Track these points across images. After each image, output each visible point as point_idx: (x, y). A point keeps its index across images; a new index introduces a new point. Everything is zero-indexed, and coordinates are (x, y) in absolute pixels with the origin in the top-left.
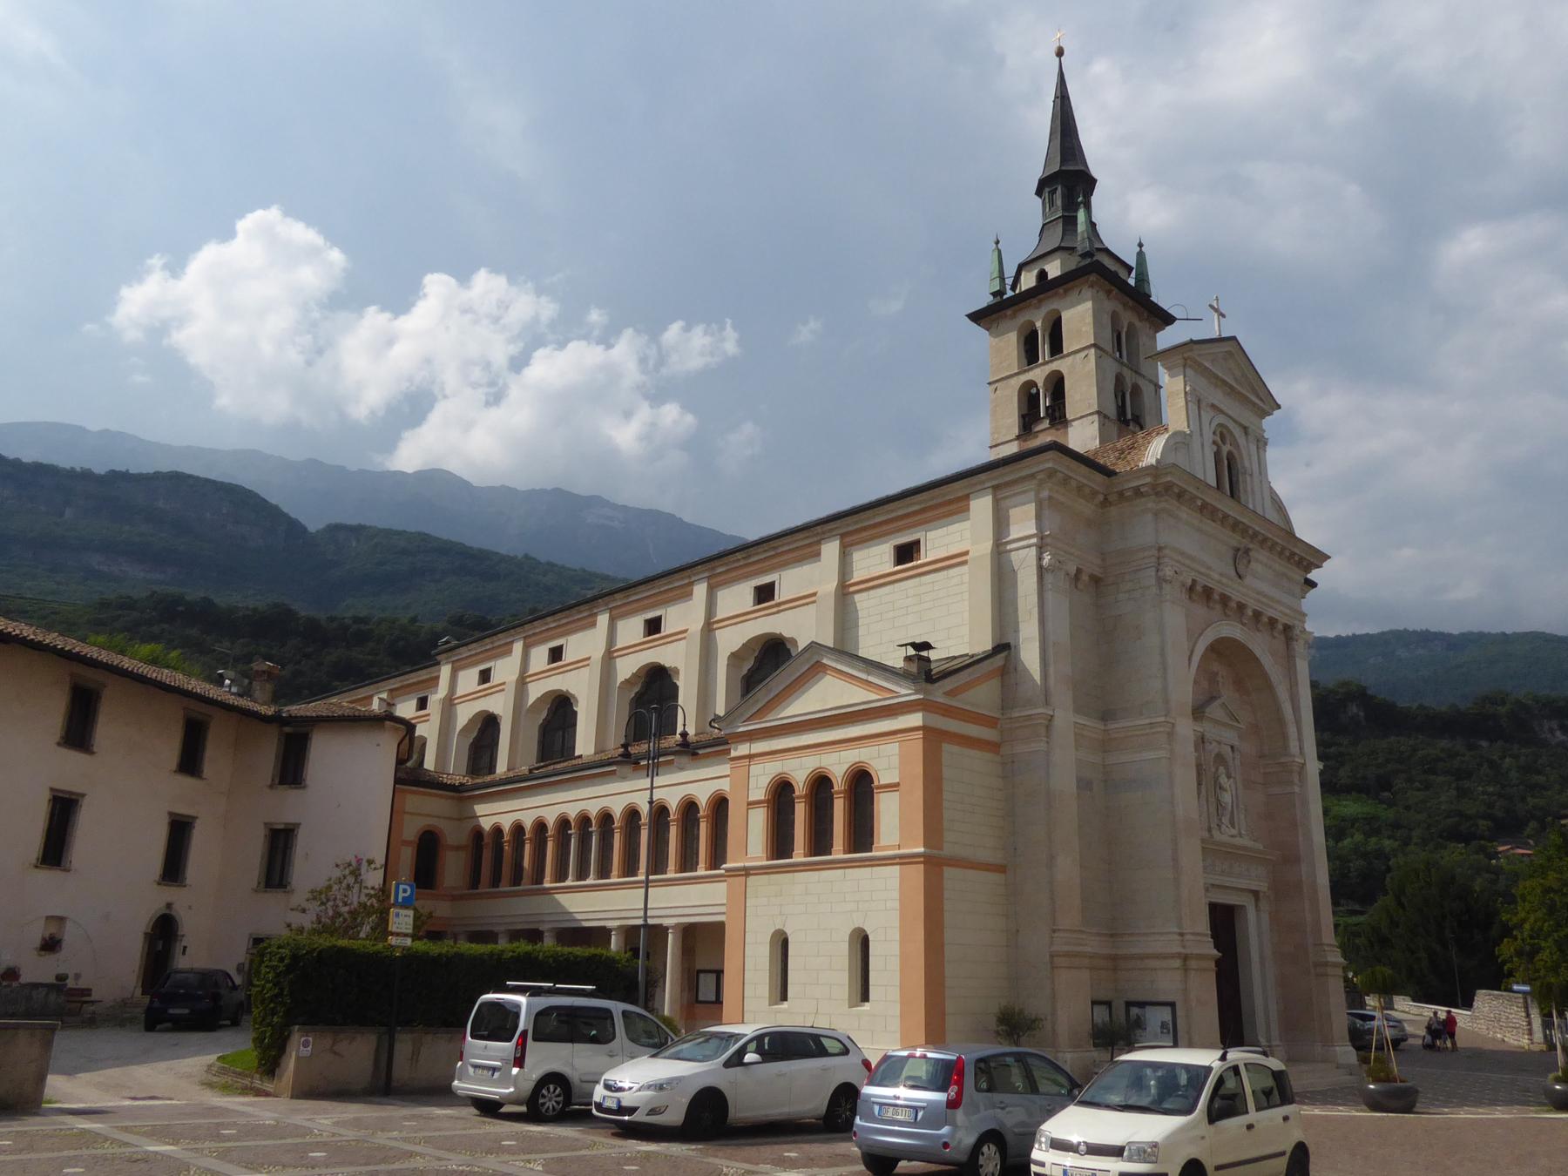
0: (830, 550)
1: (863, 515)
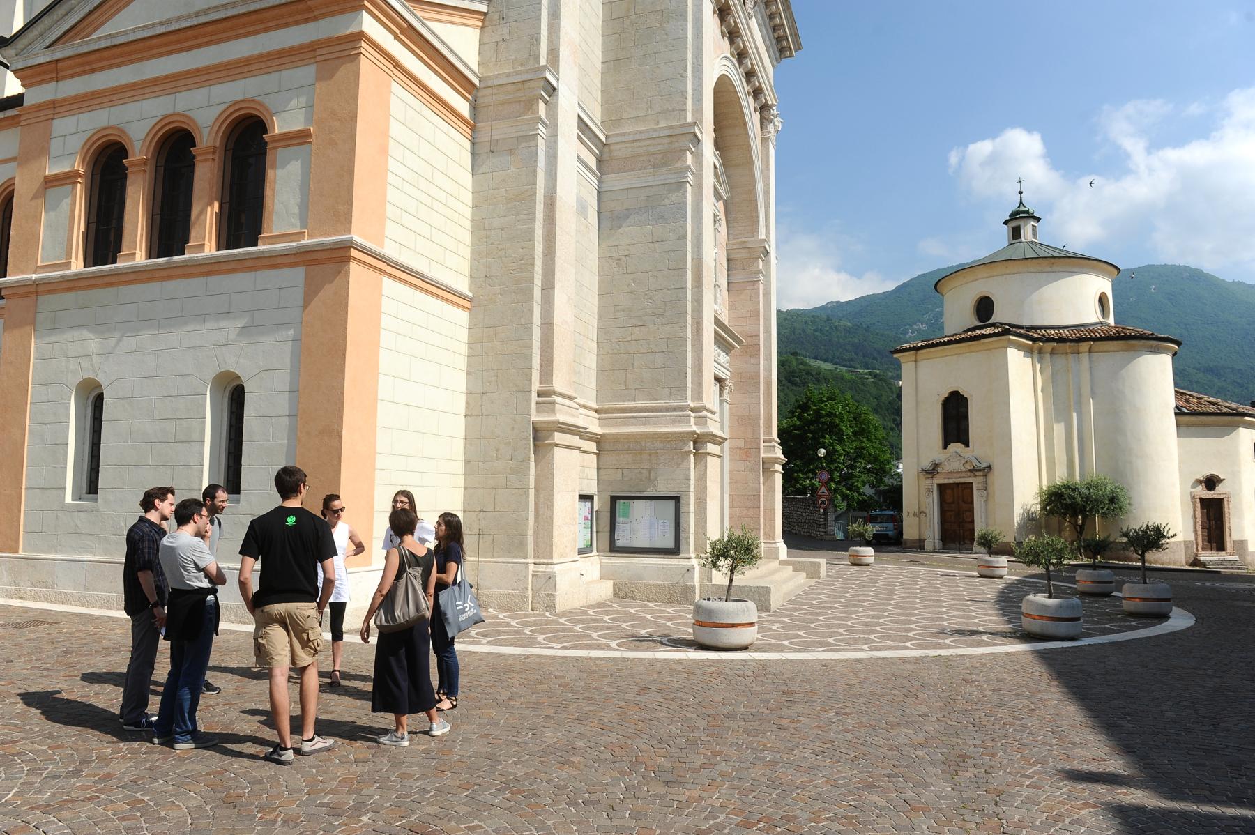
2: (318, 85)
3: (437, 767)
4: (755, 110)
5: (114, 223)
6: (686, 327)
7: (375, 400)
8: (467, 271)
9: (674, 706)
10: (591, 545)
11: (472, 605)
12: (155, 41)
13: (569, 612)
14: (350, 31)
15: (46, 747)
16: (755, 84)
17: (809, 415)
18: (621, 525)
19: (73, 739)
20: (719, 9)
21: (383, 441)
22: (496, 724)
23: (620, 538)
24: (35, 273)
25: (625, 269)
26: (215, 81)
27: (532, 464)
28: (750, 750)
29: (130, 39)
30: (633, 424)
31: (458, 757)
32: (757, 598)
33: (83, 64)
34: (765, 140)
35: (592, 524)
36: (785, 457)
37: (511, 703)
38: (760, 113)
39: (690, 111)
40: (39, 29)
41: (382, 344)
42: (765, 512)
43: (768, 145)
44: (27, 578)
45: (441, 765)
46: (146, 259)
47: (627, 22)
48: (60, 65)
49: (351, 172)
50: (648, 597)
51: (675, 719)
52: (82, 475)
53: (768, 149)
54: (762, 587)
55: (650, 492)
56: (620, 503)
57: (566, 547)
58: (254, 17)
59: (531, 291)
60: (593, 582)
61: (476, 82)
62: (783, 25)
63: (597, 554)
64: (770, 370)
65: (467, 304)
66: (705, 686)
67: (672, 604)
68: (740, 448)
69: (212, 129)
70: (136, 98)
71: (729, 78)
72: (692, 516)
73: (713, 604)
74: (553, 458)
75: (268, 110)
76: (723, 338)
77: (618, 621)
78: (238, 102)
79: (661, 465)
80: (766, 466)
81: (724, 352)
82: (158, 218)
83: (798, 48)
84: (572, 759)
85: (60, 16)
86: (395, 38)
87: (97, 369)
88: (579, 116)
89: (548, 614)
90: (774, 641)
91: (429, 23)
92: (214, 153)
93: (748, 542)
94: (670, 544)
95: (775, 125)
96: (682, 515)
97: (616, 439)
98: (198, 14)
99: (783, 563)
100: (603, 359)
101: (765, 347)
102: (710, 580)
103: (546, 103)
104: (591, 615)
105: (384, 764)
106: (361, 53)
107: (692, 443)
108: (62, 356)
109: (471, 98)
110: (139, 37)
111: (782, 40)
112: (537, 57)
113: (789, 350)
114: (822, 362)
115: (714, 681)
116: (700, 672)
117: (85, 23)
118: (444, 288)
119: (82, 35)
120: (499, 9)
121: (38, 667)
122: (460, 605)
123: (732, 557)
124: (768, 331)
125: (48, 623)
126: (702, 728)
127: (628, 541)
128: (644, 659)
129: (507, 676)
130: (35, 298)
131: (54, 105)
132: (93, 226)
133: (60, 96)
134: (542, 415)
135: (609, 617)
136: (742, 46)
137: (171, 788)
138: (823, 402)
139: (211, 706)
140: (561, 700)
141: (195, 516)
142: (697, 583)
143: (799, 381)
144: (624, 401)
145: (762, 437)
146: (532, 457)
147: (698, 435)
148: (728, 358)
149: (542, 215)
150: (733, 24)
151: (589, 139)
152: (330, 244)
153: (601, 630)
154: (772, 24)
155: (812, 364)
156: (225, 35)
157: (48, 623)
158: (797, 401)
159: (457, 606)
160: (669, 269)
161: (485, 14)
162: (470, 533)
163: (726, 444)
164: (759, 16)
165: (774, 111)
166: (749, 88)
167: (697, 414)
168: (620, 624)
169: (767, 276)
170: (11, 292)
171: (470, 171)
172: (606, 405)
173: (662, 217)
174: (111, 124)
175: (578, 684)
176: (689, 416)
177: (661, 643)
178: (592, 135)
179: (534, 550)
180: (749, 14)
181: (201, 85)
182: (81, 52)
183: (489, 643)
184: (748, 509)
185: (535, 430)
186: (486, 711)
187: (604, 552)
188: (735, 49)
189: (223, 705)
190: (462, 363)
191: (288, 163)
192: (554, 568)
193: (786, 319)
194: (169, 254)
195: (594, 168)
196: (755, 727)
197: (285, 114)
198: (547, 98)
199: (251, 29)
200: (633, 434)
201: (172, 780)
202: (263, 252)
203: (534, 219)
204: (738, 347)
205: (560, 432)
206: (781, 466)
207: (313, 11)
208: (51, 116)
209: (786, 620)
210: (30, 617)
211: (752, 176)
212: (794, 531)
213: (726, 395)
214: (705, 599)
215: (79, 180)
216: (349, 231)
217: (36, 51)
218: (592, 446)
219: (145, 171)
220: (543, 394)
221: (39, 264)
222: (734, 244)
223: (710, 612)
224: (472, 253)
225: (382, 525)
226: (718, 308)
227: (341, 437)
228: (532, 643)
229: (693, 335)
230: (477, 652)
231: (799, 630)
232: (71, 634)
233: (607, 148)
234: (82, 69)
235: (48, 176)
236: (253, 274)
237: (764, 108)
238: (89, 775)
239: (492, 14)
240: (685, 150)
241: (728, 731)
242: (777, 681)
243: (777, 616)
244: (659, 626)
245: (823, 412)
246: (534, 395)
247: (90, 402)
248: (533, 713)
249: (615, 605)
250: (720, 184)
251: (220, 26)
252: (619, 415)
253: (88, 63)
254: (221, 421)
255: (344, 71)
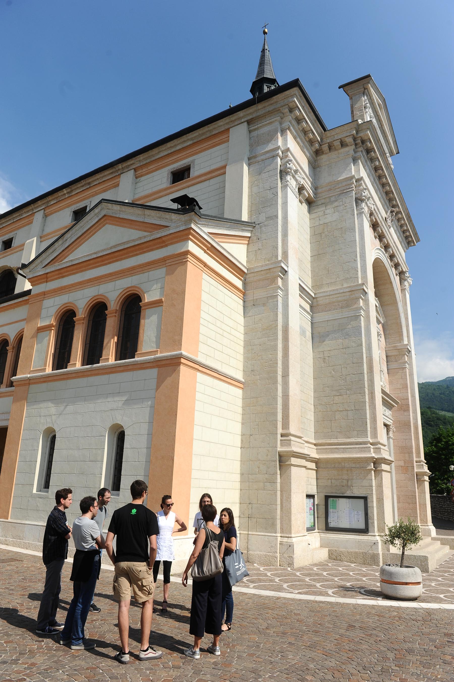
0: (38, 217)
1: (151, 153)
2: (166, 277)
3: (221, 676)
4: (397, 275)
5: (67, 349)
6: (365, 395)
7: (192, 439)
8: (241, 368)
9: (372, 641)
10: (314, 525)
11: (243, 565)
12: (91, 262)
13: (302, 568)
14: (183, 250)
15: (3, 642)
16: (395, 261)
17: (442, 444)
18: (332, 514)
19: (18, 637)
20: (372, 225)
21: (196, 463)
22: (258, 647)
23: (331, 521)
24: (29, 374)
25: (328, 364)
26: (118, 279)
27: (279, 476)
28: (426, 679)
29: (80, 262)
30: (336, 453)
31: (235, 670)
32: (420, 563)
33: (59, 274)
34: (403, 290)
35: (314, 512)
36: (430, 471)
37: (268, 631)
38: (399, 276)
39: (360, 278)
40: (40, 260)
41: (196, 408)
42: (420, 506)
43: (405, 293)
44: (11, 534)
45: (224, 675)
46: (81, 366)
47: (323, 235)
48: (48, 275)
49: (182, 319)
50: (350, 560)
51: (373, 651)
52: (42, 478)
53: (405, 295)
54: (423, 556)
55: (348, 494)
56: (330, 500)
57: (299, 527)
58: (137, 247)
59: (276, 377)
60: (316, 549)
61: (245, 271)
62: (408, 230)
63: (318, 531)
64: (417, 419)
65: (242, 386)
66: (391, 627)
67: (365, 565)
68: (402, 466)
69: (115, 301)
70: (81, 289)
71: (381, 259)
72: (375, 509)
73: (393, 569)
74: (291, 473)
75: (142, 291)
76: (387, 401)
77: (332, 576)
78: (128, 288)
79: (354, 477)
80: (418, 477)
81: (388, 409)
82: (88, 345)
83: (418, 240)
84: (306, 677)
85: (50, 253)
86: (205, 252)
87: (54, 422)
88: (300, 284)
89: (289, 569)
90: (434, 595)
91: (221, 244)
92: (116, 313)
93: (413, 529)
94: (362, 526)
95: (408, 282)
96: (369, 508)
97: (328, 461)
98: (111, 248)
99: (433, 539)
100: (317, 415)
101: (413, 406)
102: (389, 550)
103: (282, 279)
104: (315, 571)
105: (189, 670)
106: (188, 261)
107: (372, 464)
108: (38, 416)
109: (243, 279)
110: (84, 260)
111: (408, 238)
112: (277, 256)
113: (425, 406)
114: (446, 412)
115: (397, 623)
116: (387, 616)
117: (61, 255)
118: (230, 377)
119: (59, 261)
120: (257, 234)
121: (8, 588)
122: (237, 565)
123: (403, 538)
124: (413, 396)
125: (18, 560)
126: (391, 659)
127: (337, 524)
128: (350, 604)
129: (265, 612)
130: (28, 386)
131: (44, 293)
132: (58, 350)
133: (47, 289)
134: (284, 447)
135: (327, 573)
136: (386, 242)
137: (65, 677)
138: (450, 436)
139: (95, 620)
140: (298, 631)
141: (91, 508)
142: (380, 552)
143: (433, 424)
144: (331, 439)
145: (415, 459)
146: (279, 472)
147: (376, 459)
148: (391, 412)
149: (281, 337)
150: (381, 232)
151: (305, 296)
152: (170, 356)
153: (322, 582)
154: (402, 230)
155: (440, 414)
156: (123, 257)
157: (18, 560)
158: (434, 436)
159: (236, 566)
160: (353, 363)
161: (249, 237)
162: (243, 516)
163: (393, 464)
164: (395, 226)
165: (407, 275)
166: (392, 263)
167: (375, 446)
168: (333, 578)
169: (411, 365)
170: (18, 383)
171: (243, 314)
172: (320, 441)
173: (348, 335)
174: (69, 301)
175: (308, 620)
176: (370, 447)
177: (360, 593)
178: (307, 294)
179: (281, 528)
180: (389, 226)
181: (111, 281)
182: (58, 268)
183: (255, 587)
184: (409, 504)
185: (280, 456)
186: (253, 636)
187: (322, 530)
188: (383, 244)
189: (101, 620)
190: (239, 418)
191: (151, 316)
192: (292, 540)
193: (423, 388)
194: (92, 364)
195: (309, 310)
196: (427, 661)
197: (150, 292)
198: (282, 276)
199: (135, 253)
200: (337, 459)
201: (67, 671)
202: (137, 361)
203: (277, 339)
204: (396, 406)
205: (294, 457)
206: (428, 477)
207: (165, 243)
208: (43, 299)
209: (440, 579)
210: (9, 556)
211: (398, 310)
212: (438, 517)
213: (391, 434)
214: (387, 565)
215: (53, 328)
216: (180, 350)
217: (39, 269)
218: (313, 466)
219: (83, 323)
220: (284, 435)
221: (31, 369)
222: (389, 347)
223: (391, 574)
224: (244, 358)
225: (195, 510)
226: (383, 384)
227: (173, 460)
228: (279, 589)
229: (369, 400)
230: (247, 593)
231: (449, 587)
232: (28, 568)
233: (315, 300)
234: (58, 276)
235: (39, 327)
236: (132, 373)
237: (401, 274)
238: (23, 663)
239: (253, 237)
240: (359, 298)
241: (409, 663)
242: (439, 625)
243: (434, 576)
244: (358, 580)
245: (450, 443)
246: (279, 436)
247: (49, 439)
248: (281, 640)
249: (330, 565)
250: (379, 315)
251: (121, 253)
252: (328, 447)
253: (61, 273)
254: (113, 451)
255: (180, 269)
